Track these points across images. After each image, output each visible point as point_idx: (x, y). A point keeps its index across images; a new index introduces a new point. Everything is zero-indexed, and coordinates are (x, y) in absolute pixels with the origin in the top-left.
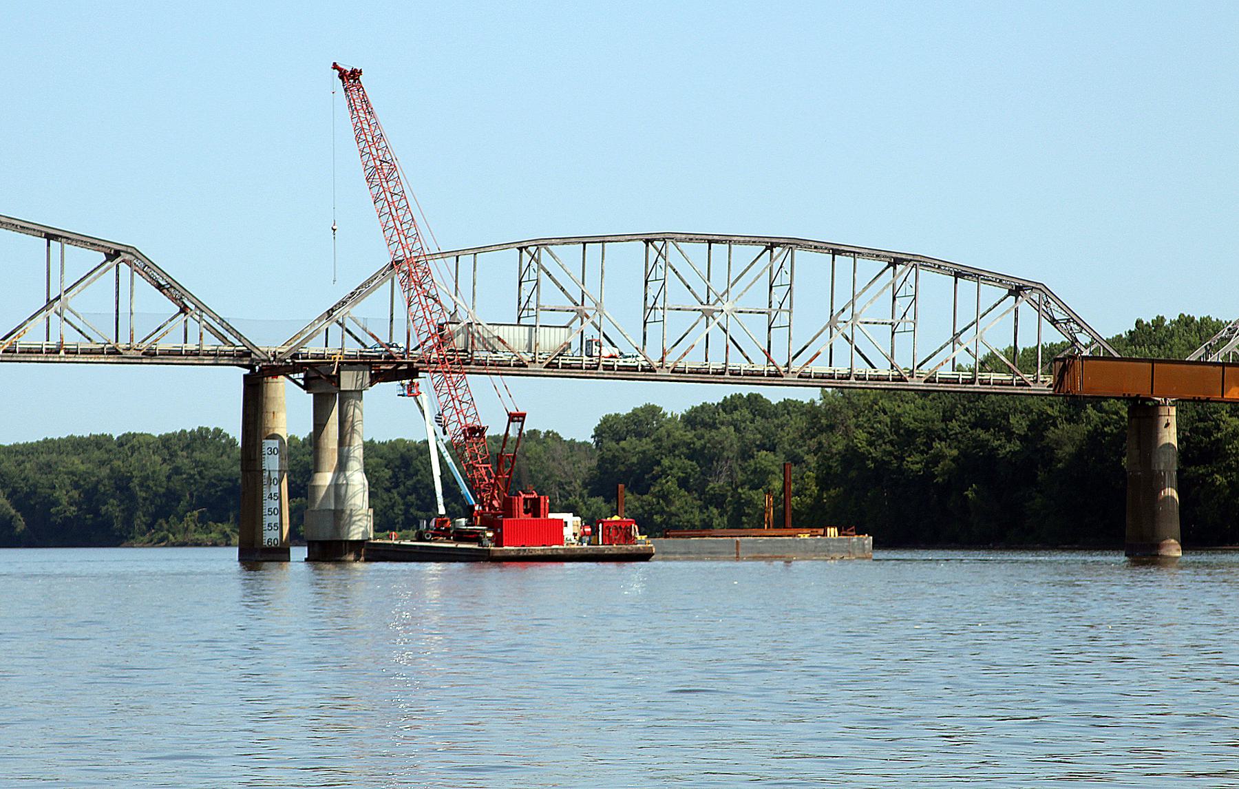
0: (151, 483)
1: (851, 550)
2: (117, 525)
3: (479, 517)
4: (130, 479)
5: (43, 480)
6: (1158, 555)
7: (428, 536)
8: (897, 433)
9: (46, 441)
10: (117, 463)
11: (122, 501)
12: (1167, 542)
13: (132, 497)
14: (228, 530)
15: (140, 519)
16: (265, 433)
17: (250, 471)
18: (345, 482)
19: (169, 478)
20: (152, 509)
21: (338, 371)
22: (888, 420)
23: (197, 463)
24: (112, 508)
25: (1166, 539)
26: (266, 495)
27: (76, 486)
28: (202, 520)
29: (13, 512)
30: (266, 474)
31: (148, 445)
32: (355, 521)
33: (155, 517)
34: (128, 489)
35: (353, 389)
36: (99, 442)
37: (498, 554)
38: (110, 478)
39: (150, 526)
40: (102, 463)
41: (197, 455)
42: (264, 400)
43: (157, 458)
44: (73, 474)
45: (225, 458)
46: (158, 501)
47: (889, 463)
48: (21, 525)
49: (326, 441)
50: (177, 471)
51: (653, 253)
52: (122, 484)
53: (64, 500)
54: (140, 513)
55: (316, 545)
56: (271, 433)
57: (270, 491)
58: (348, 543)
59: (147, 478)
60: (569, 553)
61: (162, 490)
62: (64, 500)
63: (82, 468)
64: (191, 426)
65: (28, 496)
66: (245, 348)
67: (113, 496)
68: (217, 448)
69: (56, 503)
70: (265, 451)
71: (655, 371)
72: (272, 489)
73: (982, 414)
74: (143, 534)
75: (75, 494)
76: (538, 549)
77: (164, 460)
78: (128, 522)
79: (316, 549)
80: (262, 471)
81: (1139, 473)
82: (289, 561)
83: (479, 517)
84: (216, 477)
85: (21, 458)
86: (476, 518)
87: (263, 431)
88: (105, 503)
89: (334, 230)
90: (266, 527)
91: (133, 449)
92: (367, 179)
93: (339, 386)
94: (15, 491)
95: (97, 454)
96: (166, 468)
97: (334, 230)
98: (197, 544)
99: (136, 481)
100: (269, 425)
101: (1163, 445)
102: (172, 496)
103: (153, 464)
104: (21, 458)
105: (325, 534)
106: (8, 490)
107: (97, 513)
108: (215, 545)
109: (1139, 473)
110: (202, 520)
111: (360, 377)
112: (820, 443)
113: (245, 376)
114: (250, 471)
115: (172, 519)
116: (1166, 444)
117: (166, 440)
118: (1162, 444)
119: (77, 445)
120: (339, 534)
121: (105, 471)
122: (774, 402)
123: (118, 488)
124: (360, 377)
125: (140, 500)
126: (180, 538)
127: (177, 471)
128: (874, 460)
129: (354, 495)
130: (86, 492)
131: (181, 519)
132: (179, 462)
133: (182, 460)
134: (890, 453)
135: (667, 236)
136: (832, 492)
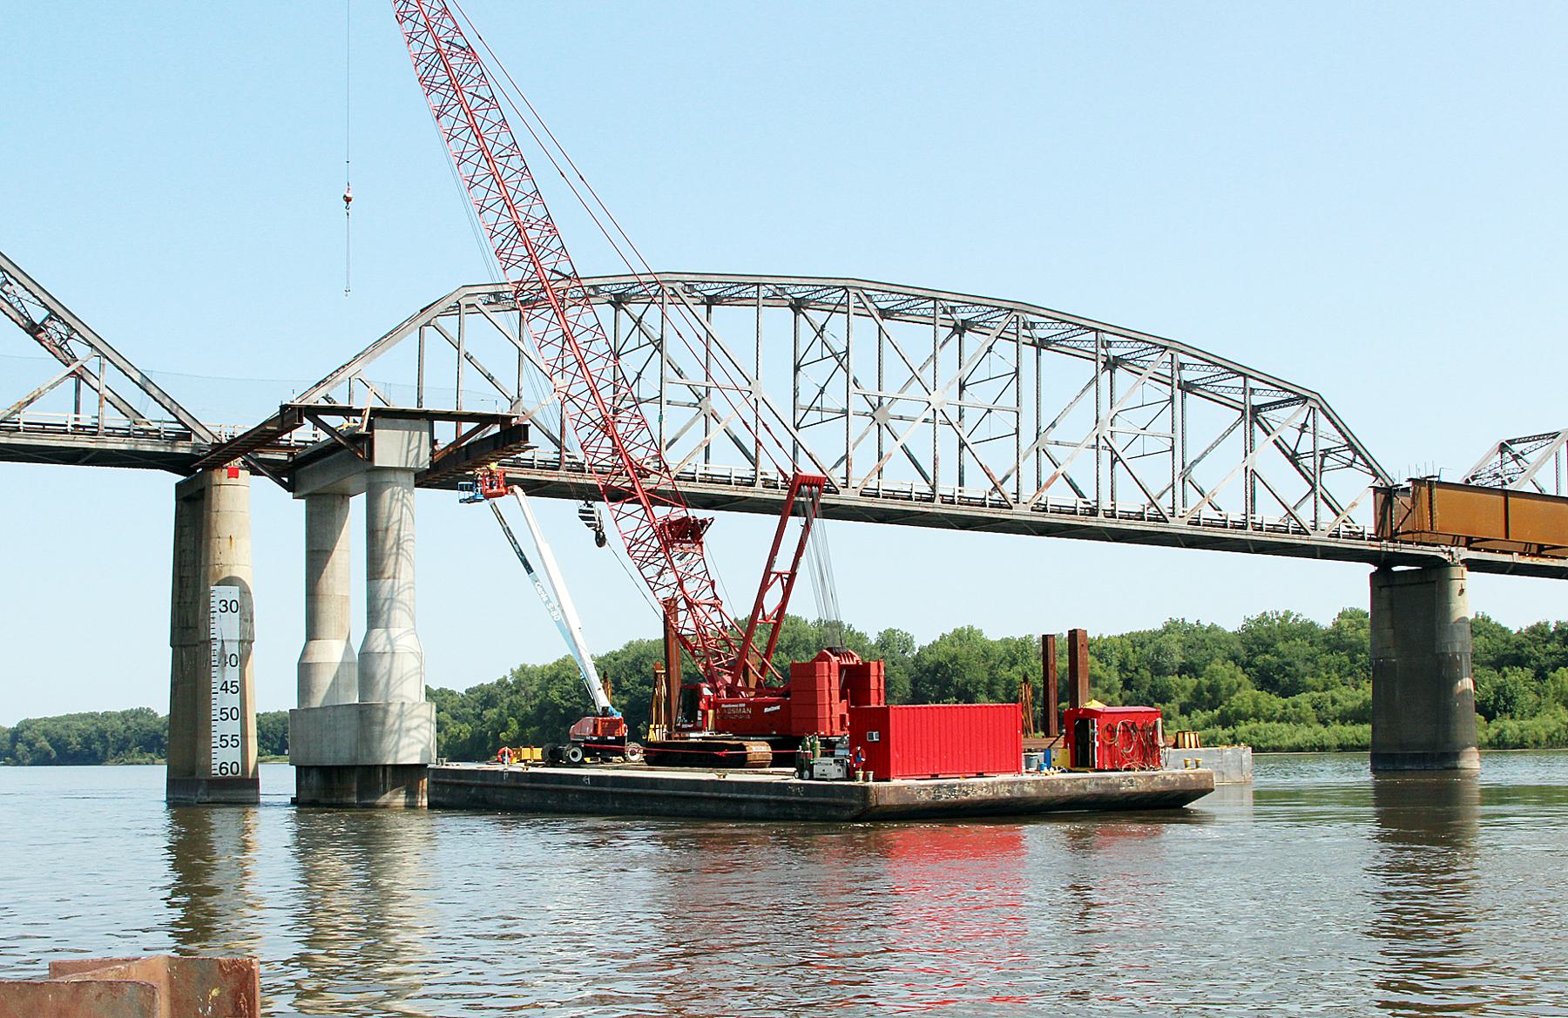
0: (116, 734)
1: (1224, 770)
2: (100, 754)
3: (711, 712)
4: (106, 732)
5: (64, 732)
6: (1456, 768)
7: (575, 755)
8: (578, 691)
9: (67, 715)
10: (99, 724)
11: (102, 743)
12: (1468, 750)
13: (107, 741)
14: (153, 756)
15: (110, 752)
16: (216, 575)
17: (185, 646)
18: (388, 648)
19: (125, 731)
20: (117, 747)
21: (371, 427)
22: (572, 683)
23: (138, 724)
24: (97, 746)
25: (1468, 746)
26: (216, 683)
27: (80, 736)
28: (141, 752)
29: (50, 748)
30: (216, 647)
31: (115, 716)
32: (409, 730)
33: (119, 750)
34: (105, 737)
35: (403, 466)
36: (92, 716)
37: (890, 800)
38: (96, 731)
39: (116, 755)
40: (93, 725)
41: (138, 720)
42: (214, 514)
43: (118, 722)
44: (79, 730)
45: (152, 722)
46: (119, 743)
47: (578, 709)
48: (54, 754)
49: (330, 581)
50: (129, 728)
51: (806, 333)
52: (102, 735)
53: (74, 743)
54: (110, 749)
55: (314, 773)
56: (225, 575)
57: (223, 677)
58: (389, 770)
59: (114, 732)
60: (1047, 793)
61: (121, 737)
62: (74, 743)
63: (84, 727)
64: (136, 707)
65: (58, 740)
66: (180, 426)
67: (98, 741)
68: (148, 716)
69: (71, 744)
70: (215, 605)
71: (837, 492)
72: (227, 673)
73: (646, 677)
74: (112, 759)
75: (79, 739)
76: (981, 787)
77: (123, 723)
78: (105, 752)
79: (314, 779)
80: (208, 642)
81: (1394, 660)
82: (256, 803)
83: (711, 712)
84: (148, 730)
85: (55, 723)
86: (705, 714)
87: (212, 569)
88: (94, 744)
89: (348, 200)
90: (216, 741)
91: (108, 718)
92: (421, 80)
93: (371, 458)
94: (52, 738)
95: (90, 721)
96: (124, 727)
97: (348, 200)
98: (139, 764)
99: (109, 733)
100: (222, 561)
101: (1459, 619)
102: (127, 741)
103: (117, 724)
104: (55, 723)
105: (338, 751)
106: (48, 738)
107: (89, 748)
108: (147, 764)
109: (1394, 660)
110: (141, 752)
111: (415, 443)
112: (511, 701)
113: (178, 486)
114: (185, 646)
115: (126, 751)
116: (1461, 618)
117: (124, 714)
118: (1456, 618)
119: (83, 717)
120: (371, 753)
121: (94, 728)
122: (435, 689)
123: (100, 736)
124: (415, 443)
125: (111, 743)
126: (130, 761)
127: (129, 728)
128: (565, 708)
129: (402, 680)
130: (85, 739)
131: (131, 751)
132: (129, 724)
133: (131, 723)
134: (579, 703)
135: (850, 283)
136: (533, 729)
